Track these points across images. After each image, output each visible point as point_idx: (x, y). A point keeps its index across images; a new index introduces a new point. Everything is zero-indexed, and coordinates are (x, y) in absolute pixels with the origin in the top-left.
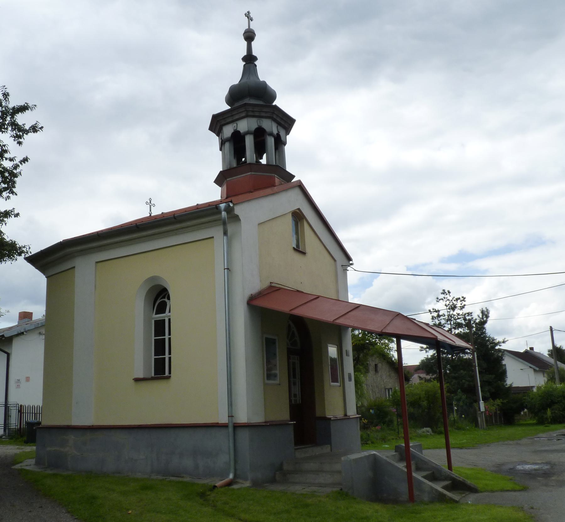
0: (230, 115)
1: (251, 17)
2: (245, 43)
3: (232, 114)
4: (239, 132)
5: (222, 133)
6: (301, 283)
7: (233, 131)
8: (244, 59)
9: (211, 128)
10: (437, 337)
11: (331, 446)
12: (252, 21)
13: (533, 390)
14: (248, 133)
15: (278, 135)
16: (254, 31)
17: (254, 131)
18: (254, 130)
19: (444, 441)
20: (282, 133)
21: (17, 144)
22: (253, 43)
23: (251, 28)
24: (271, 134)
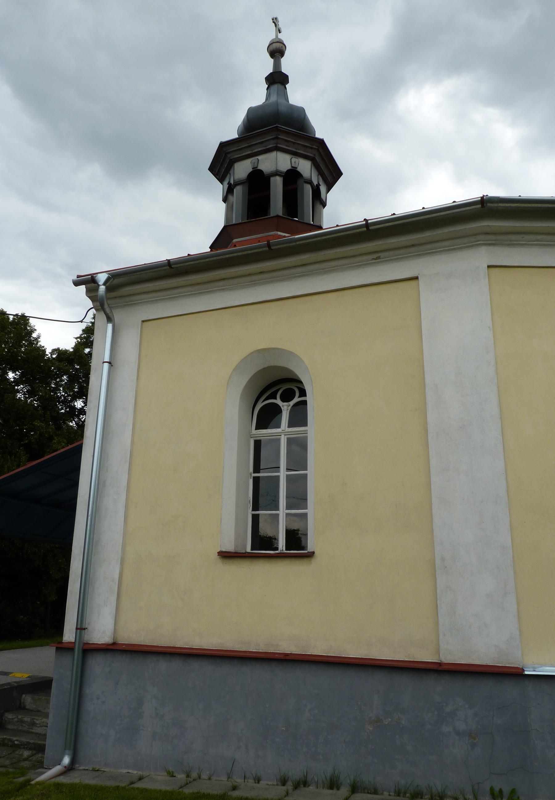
4: (261, 172)
5: (230, 174)
7: (251, 170)
9: (211, 169)
10: (58, 349)
11: (207, 780)
12: (280, 32)
13: (61, 354)
14: (277, 173)
15: (318, 185)
16: (283, 41)
17: (285, 172)
18: (285, 170)
20: (323, 189)
24: (310, 182)
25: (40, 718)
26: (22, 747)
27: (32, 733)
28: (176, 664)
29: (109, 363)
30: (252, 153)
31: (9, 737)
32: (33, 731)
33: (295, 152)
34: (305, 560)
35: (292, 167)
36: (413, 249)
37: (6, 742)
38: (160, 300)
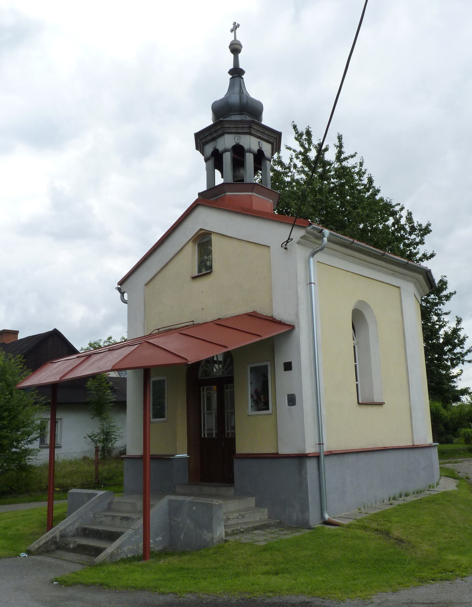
0: (207, 134)
1: (233, 26)
2: (232, 55)
3: (211, 132)
6: (203, 309)
8: (231, 72)
19: (140, 505)
21: (428, 260)
22: (240, 55)
23: (237, 39)
24: (250, 151)
25: (232, 514)
26: (245, 531)
27: (229, 525)
28: (355, 456)
29: (311, 283)
30: (261, 137)
31: (236, 528)
32: (228, 524)
33: (237, 132)
34: (381, 405)
35: (236, 143)
36: (402, 275)
37: (235, 531)
38: (337, 257)
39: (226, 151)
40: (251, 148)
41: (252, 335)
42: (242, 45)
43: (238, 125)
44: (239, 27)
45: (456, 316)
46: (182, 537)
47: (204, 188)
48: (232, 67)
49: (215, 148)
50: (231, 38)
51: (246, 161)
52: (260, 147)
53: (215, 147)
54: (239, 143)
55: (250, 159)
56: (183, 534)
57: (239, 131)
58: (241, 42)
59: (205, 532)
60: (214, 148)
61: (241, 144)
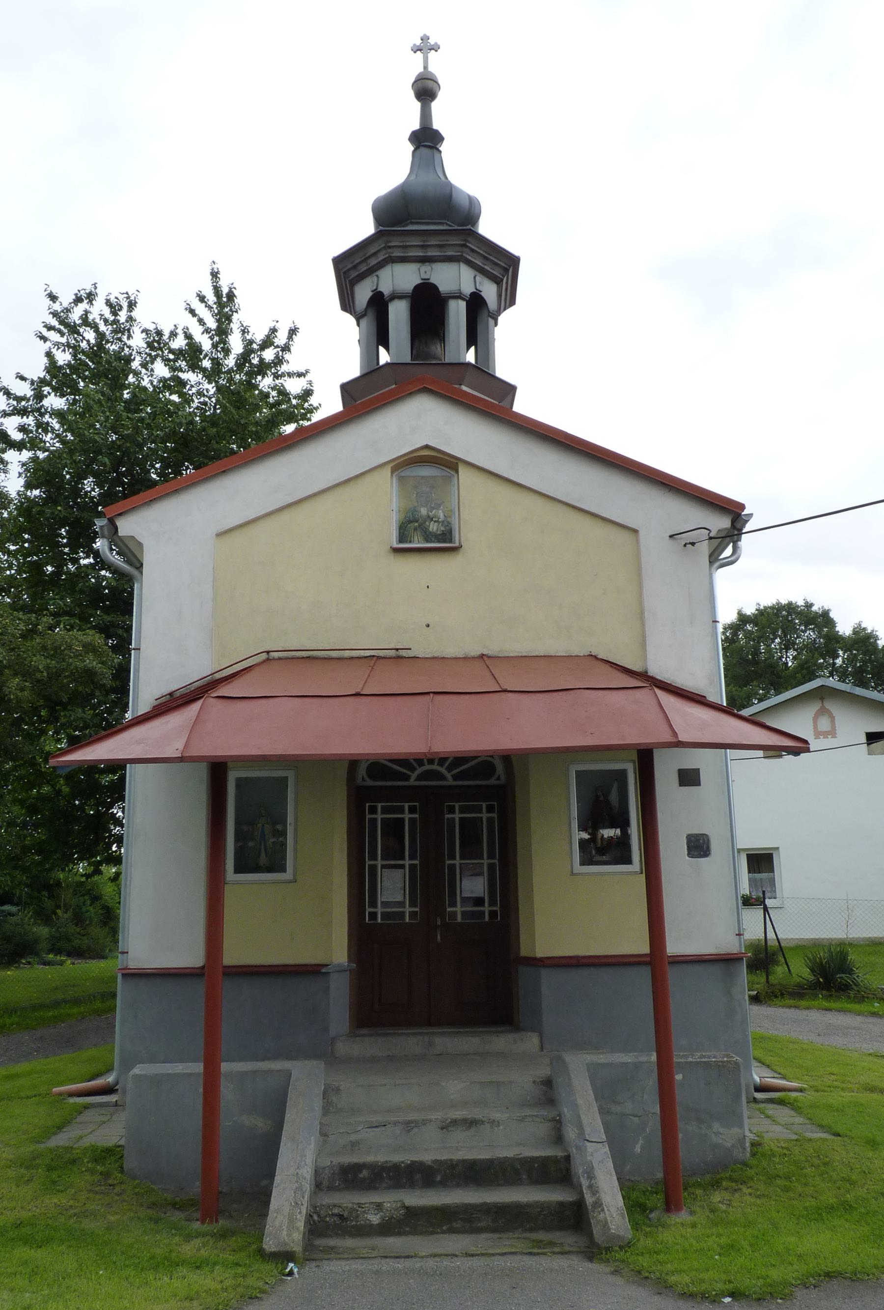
2: (418, 105)
22: (435, 105)
23: (430, 69)
35: (422, 279)
39: (395, 296)
40: (462, 289)
41: (312, 698)
42: (440, 82)
43: (491, 255)
44: (436, 51)
45: (430, 625)
46: (638, 1149)
47: (353, 371)
48: (416, 126)
49: (376, 289)
50: (414, 66)
51: (448, 320)
52: (476, 289)
53: (375, 288)
54: (428, 279)
55: (457, 312)
56: (641, 1142)
57: (486, 267)
58: (438, 77)
59: (716, 1126)
60: (372, 291)
61: (432, 281)
